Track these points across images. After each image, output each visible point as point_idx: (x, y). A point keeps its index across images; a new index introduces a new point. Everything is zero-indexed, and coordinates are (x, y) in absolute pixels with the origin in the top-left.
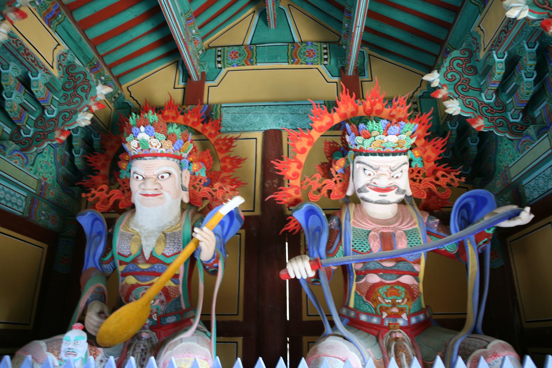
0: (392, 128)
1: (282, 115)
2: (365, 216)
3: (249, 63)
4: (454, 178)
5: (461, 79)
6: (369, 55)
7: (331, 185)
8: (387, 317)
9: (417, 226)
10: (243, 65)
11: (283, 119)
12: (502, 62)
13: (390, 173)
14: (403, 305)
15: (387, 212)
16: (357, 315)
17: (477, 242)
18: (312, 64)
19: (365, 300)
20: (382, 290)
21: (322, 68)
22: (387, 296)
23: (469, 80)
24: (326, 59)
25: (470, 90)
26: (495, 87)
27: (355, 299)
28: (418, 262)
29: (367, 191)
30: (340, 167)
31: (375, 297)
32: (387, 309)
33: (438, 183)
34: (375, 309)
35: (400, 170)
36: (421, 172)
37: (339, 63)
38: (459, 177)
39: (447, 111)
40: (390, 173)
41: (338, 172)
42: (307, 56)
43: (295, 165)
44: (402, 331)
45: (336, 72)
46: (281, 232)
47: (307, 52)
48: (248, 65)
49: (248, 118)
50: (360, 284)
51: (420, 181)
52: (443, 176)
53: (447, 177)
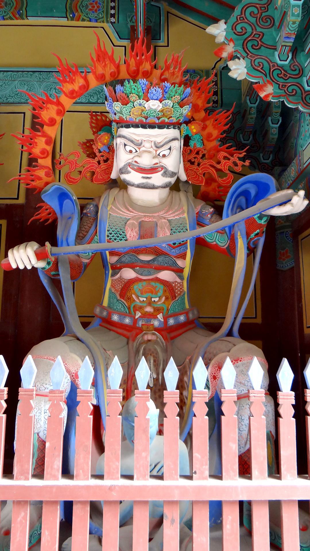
0: (152, 90)
1: (54, 84)
2: (131, 204)
3: (17, 16)
4: (238, 162)
5: (252, 32)
6: (168, 12)
7: (93, 166)
8: (140, 317)
9: (186, 215)
10: (11, 19)
11: (55, 89)
12: (298, 6)
13: (156, 151)
14: (159, 304)
15: (153, 197)
16: (110, 314)
17: (248, 235)
18: (96, 21)
19: (119, 298)
20: (137, 287)
21: (108, 26)
22: (142, 293)
23: (263, 34)
24: (113, 16)
25: (262, 48)
26: (290, 42)
27: (109, 297)
28: (183, 256)
29: (128, 172)
30: (104, 144)
31: (129, 295)
32: (141, 308)
33: (218, 166)
34: (129, 308)
35: (168, 146)
36: (200, 152)
37: (128, 20)
38: (243, 159)
39: (230, 74)
40: (156, 151)
41: (102, 150)
42: (90, 10)
43: (44, 139)
44: (156, 333)
45: (125, 32)
46: (30, 221)
47: (91, 4)
48: (17, 19)
49: (13, 86)
50: (115, 280)
51: (199, 165)
52: (225, 158)
53: (229, 159)
